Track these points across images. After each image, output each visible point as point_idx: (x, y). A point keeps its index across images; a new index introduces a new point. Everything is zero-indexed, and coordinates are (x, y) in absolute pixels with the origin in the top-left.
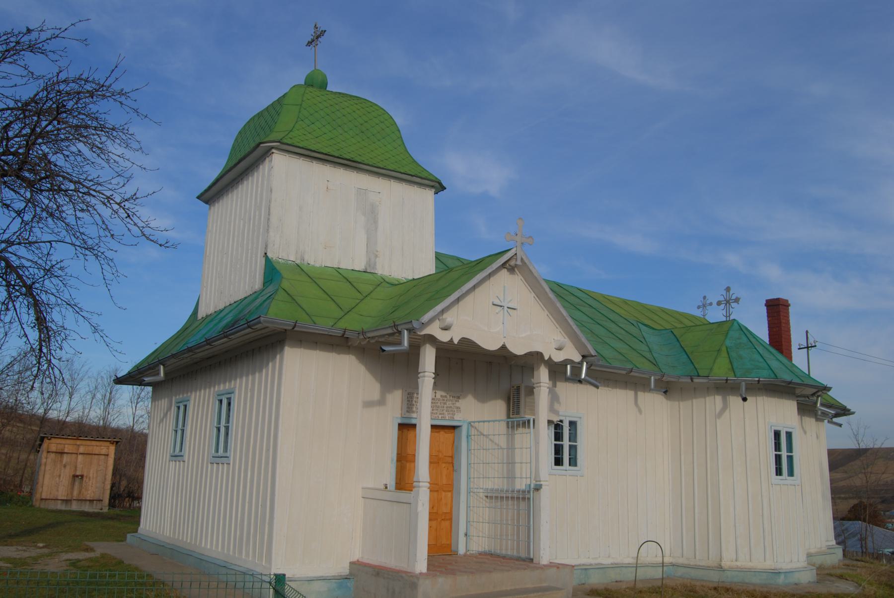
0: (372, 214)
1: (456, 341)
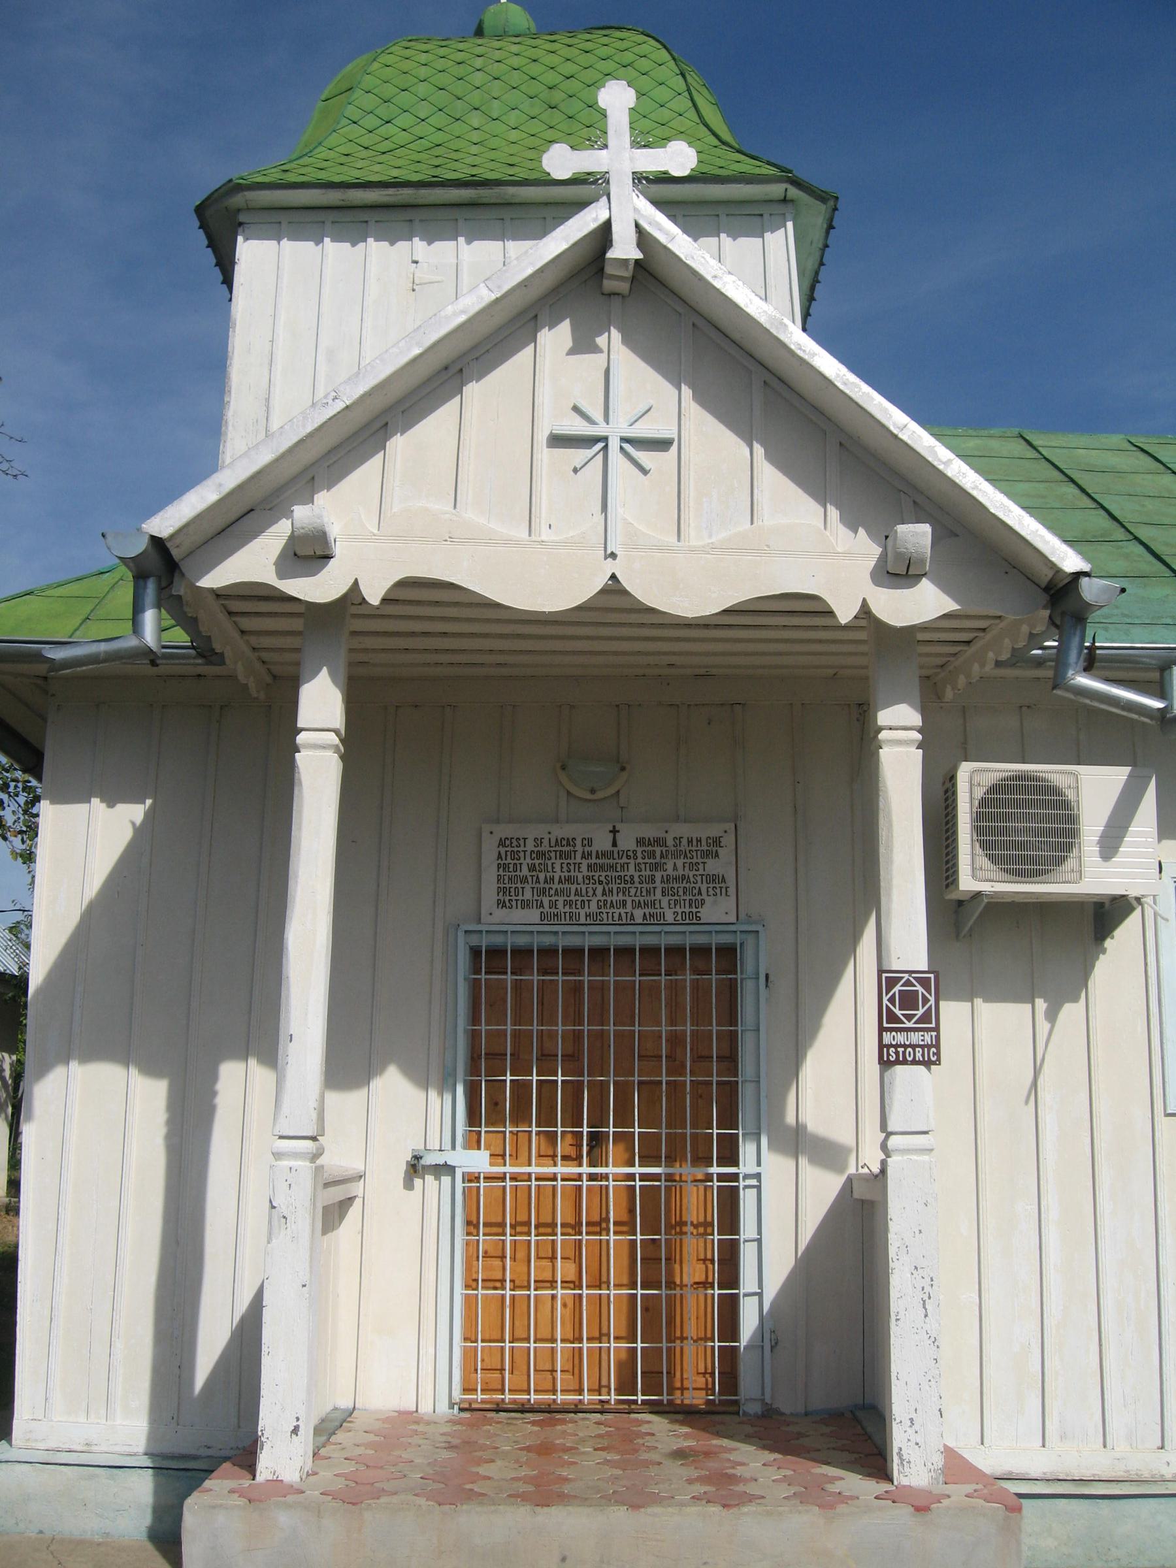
1: (373, 595)
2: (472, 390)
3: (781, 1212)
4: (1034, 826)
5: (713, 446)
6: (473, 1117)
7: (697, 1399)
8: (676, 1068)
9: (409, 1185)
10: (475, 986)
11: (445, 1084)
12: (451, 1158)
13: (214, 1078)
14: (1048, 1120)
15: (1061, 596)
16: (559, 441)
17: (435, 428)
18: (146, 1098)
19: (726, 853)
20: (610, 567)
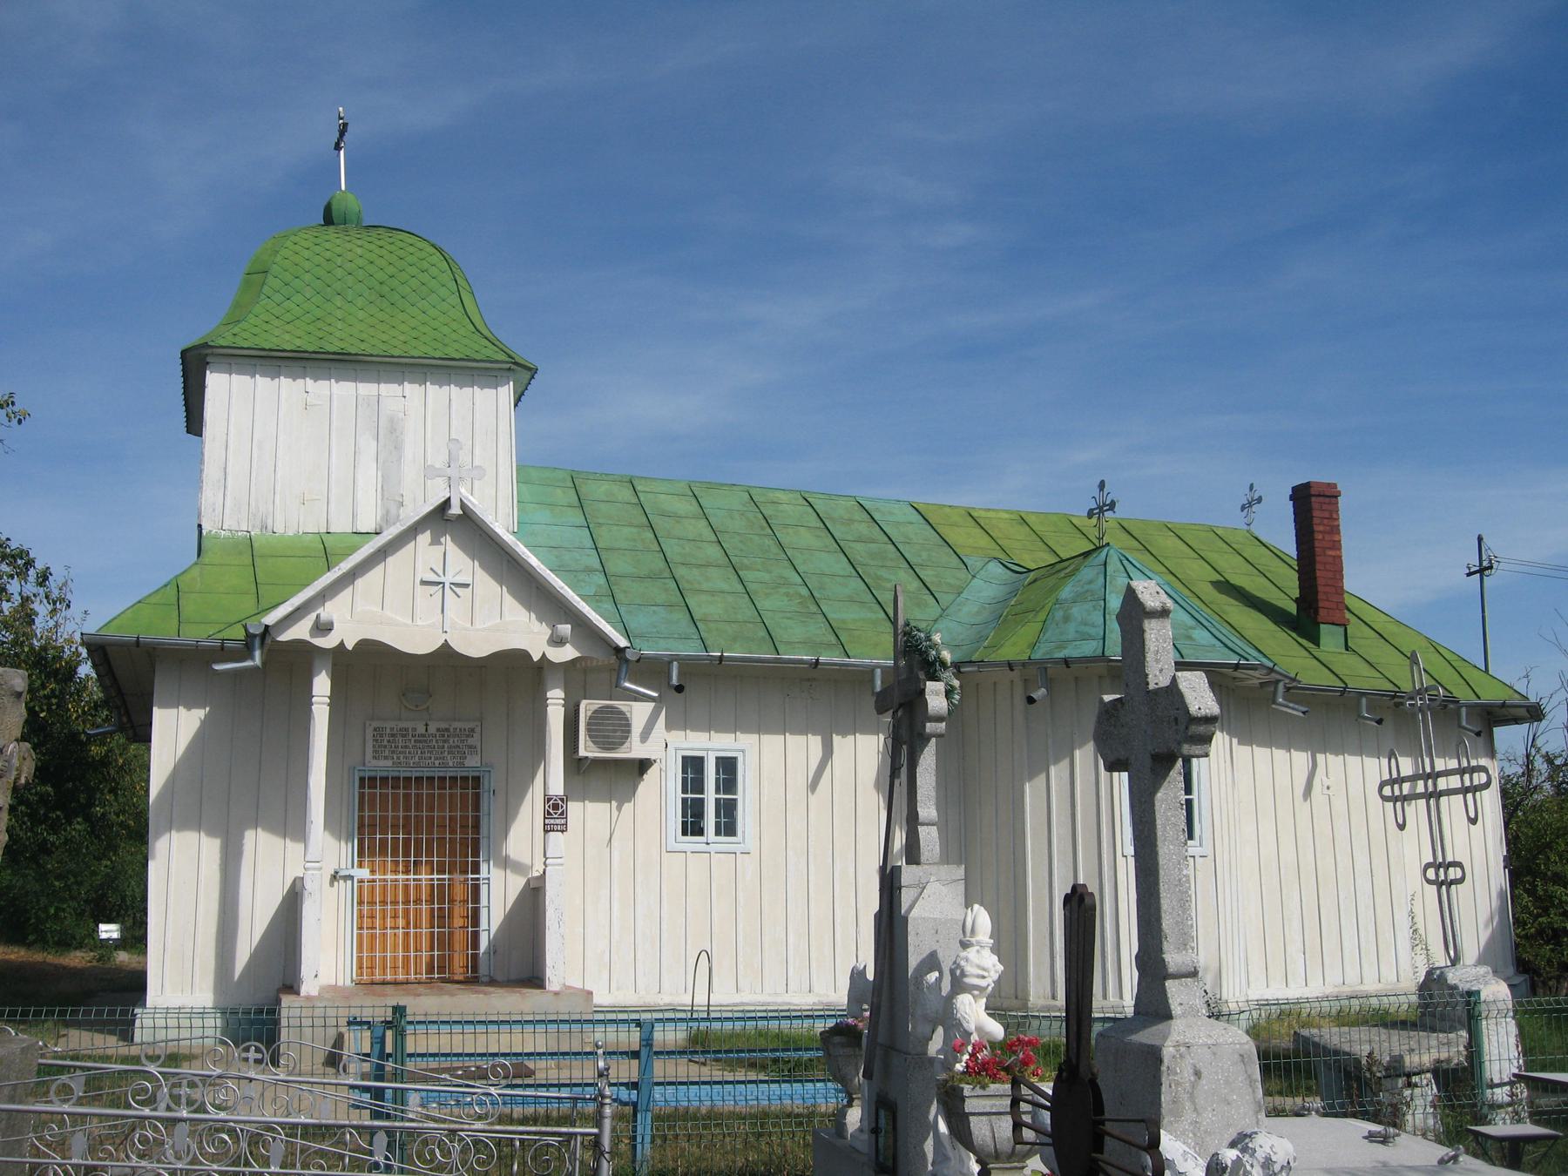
0: (390, 435)
1: (350, 646)
2: (390, 560)
3: (499, 894)
4: (612, 728)
5: (487, 587)
6: (361, 854)
7: (461, 978)
8: (453, 831)
9: (332, 884)
10: (362, 796)
11: (349, 838)
12: (352, 872)
13: (242, 837)
14: (616, 854)
15: (619, 651)
16: (423, 583)
17: (375, 574)
18: (210, 848)
19: (477, 736)
20: (444, 637)
